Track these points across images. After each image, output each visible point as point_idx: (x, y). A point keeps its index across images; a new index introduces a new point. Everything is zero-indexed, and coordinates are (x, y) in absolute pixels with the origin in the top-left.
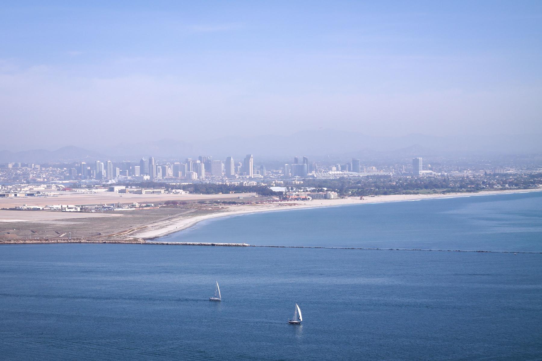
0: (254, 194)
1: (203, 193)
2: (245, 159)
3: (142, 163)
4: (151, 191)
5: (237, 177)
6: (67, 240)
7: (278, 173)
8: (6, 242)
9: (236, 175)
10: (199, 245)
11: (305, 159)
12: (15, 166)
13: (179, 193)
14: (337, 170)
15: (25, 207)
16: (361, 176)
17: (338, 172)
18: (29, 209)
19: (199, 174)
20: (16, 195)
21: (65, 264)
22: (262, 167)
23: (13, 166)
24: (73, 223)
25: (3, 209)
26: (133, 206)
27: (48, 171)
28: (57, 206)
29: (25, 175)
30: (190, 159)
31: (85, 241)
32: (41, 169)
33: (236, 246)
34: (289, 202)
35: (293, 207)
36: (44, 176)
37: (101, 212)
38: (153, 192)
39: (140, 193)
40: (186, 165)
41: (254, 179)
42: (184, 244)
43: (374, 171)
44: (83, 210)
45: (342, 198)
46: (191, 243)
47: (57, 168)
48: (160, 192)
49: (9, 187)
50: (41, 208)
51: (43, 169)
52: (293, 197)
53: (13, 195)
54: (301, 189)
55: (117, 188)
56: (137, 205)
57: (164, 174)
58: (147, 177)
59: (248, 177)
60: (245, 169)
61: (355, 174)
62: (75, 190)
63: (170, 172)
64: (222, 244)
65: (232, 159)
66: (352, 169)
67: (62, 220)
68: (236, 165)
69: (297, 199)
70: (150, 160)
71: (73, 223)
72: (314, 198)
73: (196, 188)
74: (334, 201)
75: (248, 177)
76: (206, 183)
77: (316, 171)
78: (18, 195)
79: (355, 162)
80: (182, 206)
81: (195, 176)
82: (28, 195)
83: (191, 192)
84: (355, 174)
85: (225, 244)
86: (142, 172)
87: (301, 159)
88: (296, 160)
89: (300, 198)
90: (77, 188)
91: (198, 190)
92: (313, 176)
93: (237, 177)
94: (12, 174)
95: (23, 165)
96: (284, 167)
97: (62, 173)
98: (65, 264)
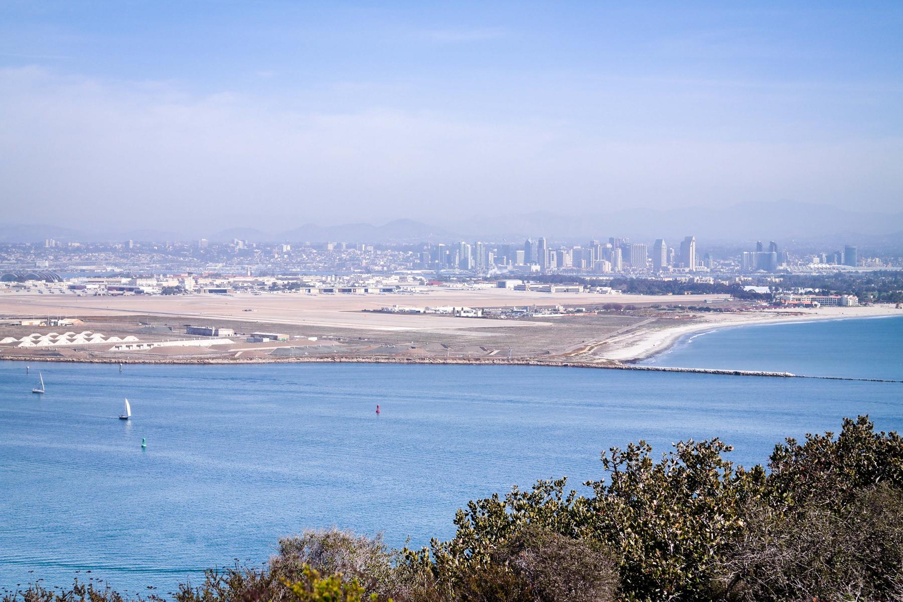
0: (728, 296)
1: (646, 293)
2: (682, 243)
3: (527, 247)
4: (565, 288)
5: (671, 270)
6: (508, 360)
7: (729, 265)
8: (418, 361)
9: (670, 267)
10: (714, 373)
11: (773, 246)
12: (338, 247)
13: (606, 292)
14: (821, 262)
15: (397, 309)
16: (860, 271)
17: (824, 266)
18: (402, 312)
19: (615, 265)
20: (366, 291)
21: (111, 379)
22: (707, 256)
23: (335, 247)
24: (489, 334)
25: (365, 311)
26: (556, 311)
27: (386, 255)
28: (445, 309)
29: (355, 261)
30: (596, 242)
31: (536, 363)
32: (375, 252)
33: (773, 376)
34: (788, 310)
35: (800, 318)
36: (382, 263)
37: (513, 319)
38: (567, 291)
39: (549, 291)
40: (593, 251)
41: (697, 273)
42: (691, 372)
43: (878, 265)
44: (486, 315)
45: (865, 305)
46: (702, 370)
47: (399, 251)
48: (577, 291)
49: (345, 278)
50: (422, 311)
51: (379, 252)
52: (791, 302)
53: (363, 291)
54: (790, 290)
55: (511, 284)
56: (562, 309)
57: (560, 263)
58: (536, 268)
59: (687, 270)
60: (682, 258)
61: (849, 268)
62: (448, 284)
63: (568, 260)
64: (751, 372)
65: (663, 243)
66: (843, 261)
67: (470, 330)
68: (669, 252)
69: (795, 305)
70: (541, 242)
71: (489, 334)
72: (823, 304)
73: (632, 287)
74: (853, 310)
75: (687, 270)
76: (632, 279)
77: (788, 263)
78: (370, 291)
79: (849, 251)
80: (631, 312)
81: (607, 267)
82: (385, 290)
83: (624, 292)
84: (849, 268)
85: (756, 372)
86: (528, 259)
87: (766, 245)
88: (759, 247)
89: (802, 305)
90: (446, 281)
91: (636, 288)
92: (787, 271)
93: (671, 270)
94: (335, 258)
95: (348, 247)
96: (742, 255)
97: (407, 260)
98: (111, 379)
